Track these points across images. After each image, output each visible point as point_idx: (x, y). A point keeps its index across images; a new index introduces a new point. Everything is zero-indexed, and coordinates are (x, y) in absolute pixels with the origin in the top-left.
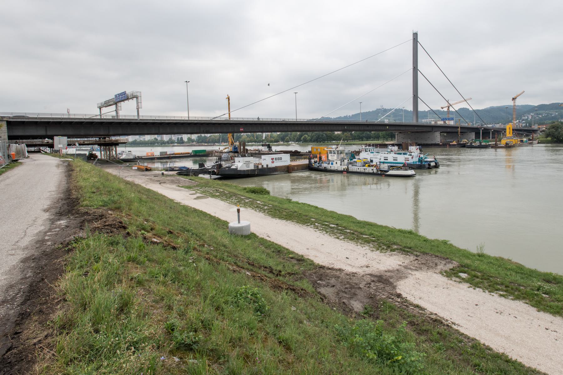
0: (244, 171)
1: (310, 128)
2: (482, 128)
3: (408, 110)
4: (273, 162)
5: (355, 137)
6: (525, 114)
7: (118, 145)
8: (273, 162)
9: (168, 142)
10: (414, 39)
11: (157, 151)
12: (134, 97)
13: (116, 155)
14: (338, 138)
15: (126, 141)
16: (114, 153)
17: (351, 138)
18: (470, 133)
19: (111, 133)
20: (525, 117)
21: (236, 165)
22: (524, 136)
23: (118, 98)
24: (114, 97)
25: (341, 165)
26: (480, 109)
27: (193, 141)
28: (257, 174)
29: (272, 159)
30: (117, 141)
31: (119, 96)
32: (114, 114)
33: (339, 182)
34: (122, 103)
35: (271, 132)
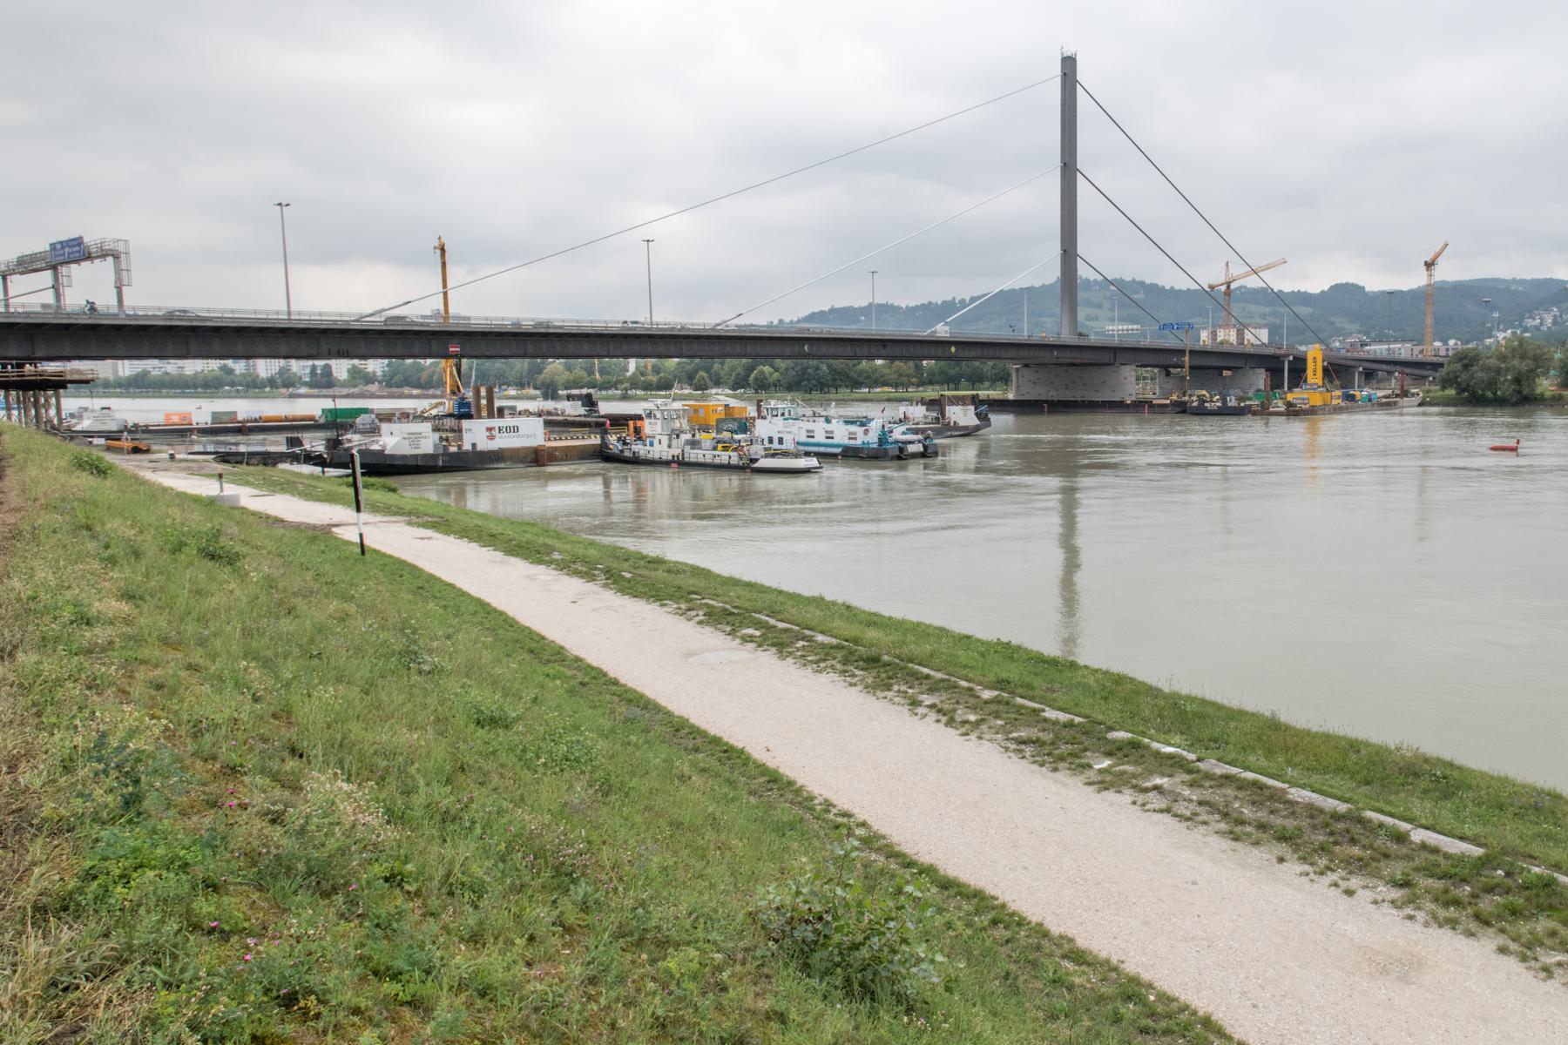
0: (404, 457)
1: (684, 348)
2: (1288, 355)
3: (1163, 287)
4: (491, 438)
5: (934, 375)
6: (1537, 309)
7: (65, 387)
8: (491, 438)
9: (271, 382)
10: (1064, 75)
11: (201, 411)
12: (107, 255)
13: (60, 420)
14: (875, 381)
15: (90, 377)
16: (52, 412)
17: (914, 380)
18: (1251, 372)
19: (39, 354)
20: (1534, 319)
21: (381, 443)
22: (1430, 382)
23: (61, 252)
24: (48, 249)
25: (669, 446)
26: (1405, 289)
27: (369, 379)
28: (443, 467)
29: (490, 429)
30: (60, 374)
31: (63, 248)
32: (48, 297)
33: (667, 486)
34: (73, 266)
35: (660, 356)
